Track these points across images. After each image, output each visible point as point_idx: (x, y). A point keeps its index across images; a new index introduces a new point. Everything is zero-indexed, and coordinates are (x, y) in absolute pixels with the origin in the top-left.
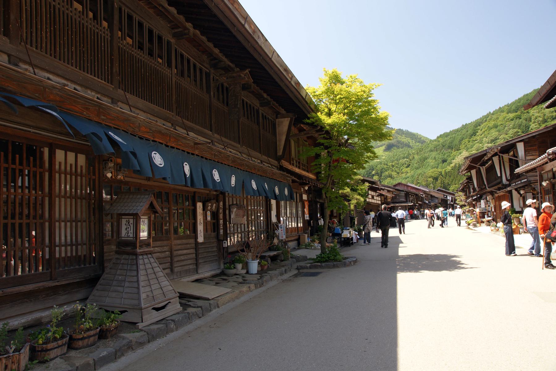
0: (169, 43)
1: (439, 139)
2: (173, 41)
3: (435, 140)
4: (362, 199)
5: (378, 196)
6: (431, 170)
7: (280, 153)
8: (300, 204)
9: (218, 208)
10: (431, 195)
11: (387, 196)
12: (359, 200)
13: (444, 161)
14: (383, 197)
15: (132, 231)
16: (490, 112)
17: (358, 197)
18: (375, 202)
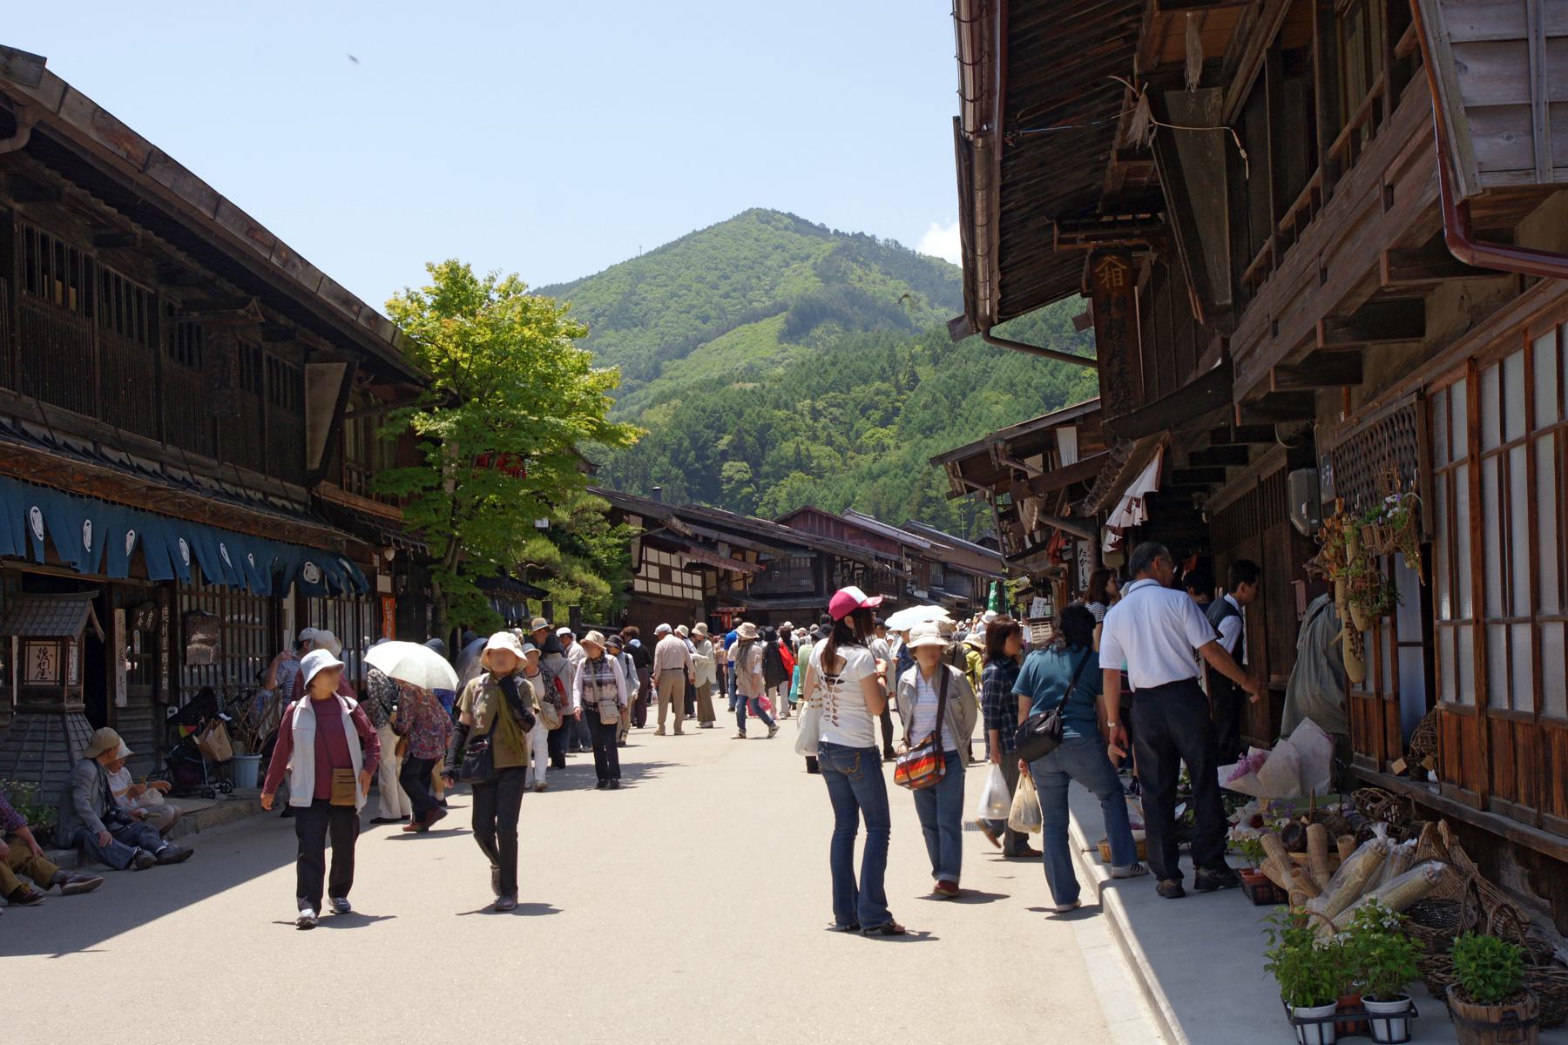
0: (88, 260)
2: (93, 254)
4: (604, 587)
5: (691, 568)
7: (315, 463)
8: (367, 607)
9: (158, 622)
10: (944, 565)
11: (728, 572)
14: (711, 576)
15: (52, 669)
17: (591, 578)
18: (677, 592)
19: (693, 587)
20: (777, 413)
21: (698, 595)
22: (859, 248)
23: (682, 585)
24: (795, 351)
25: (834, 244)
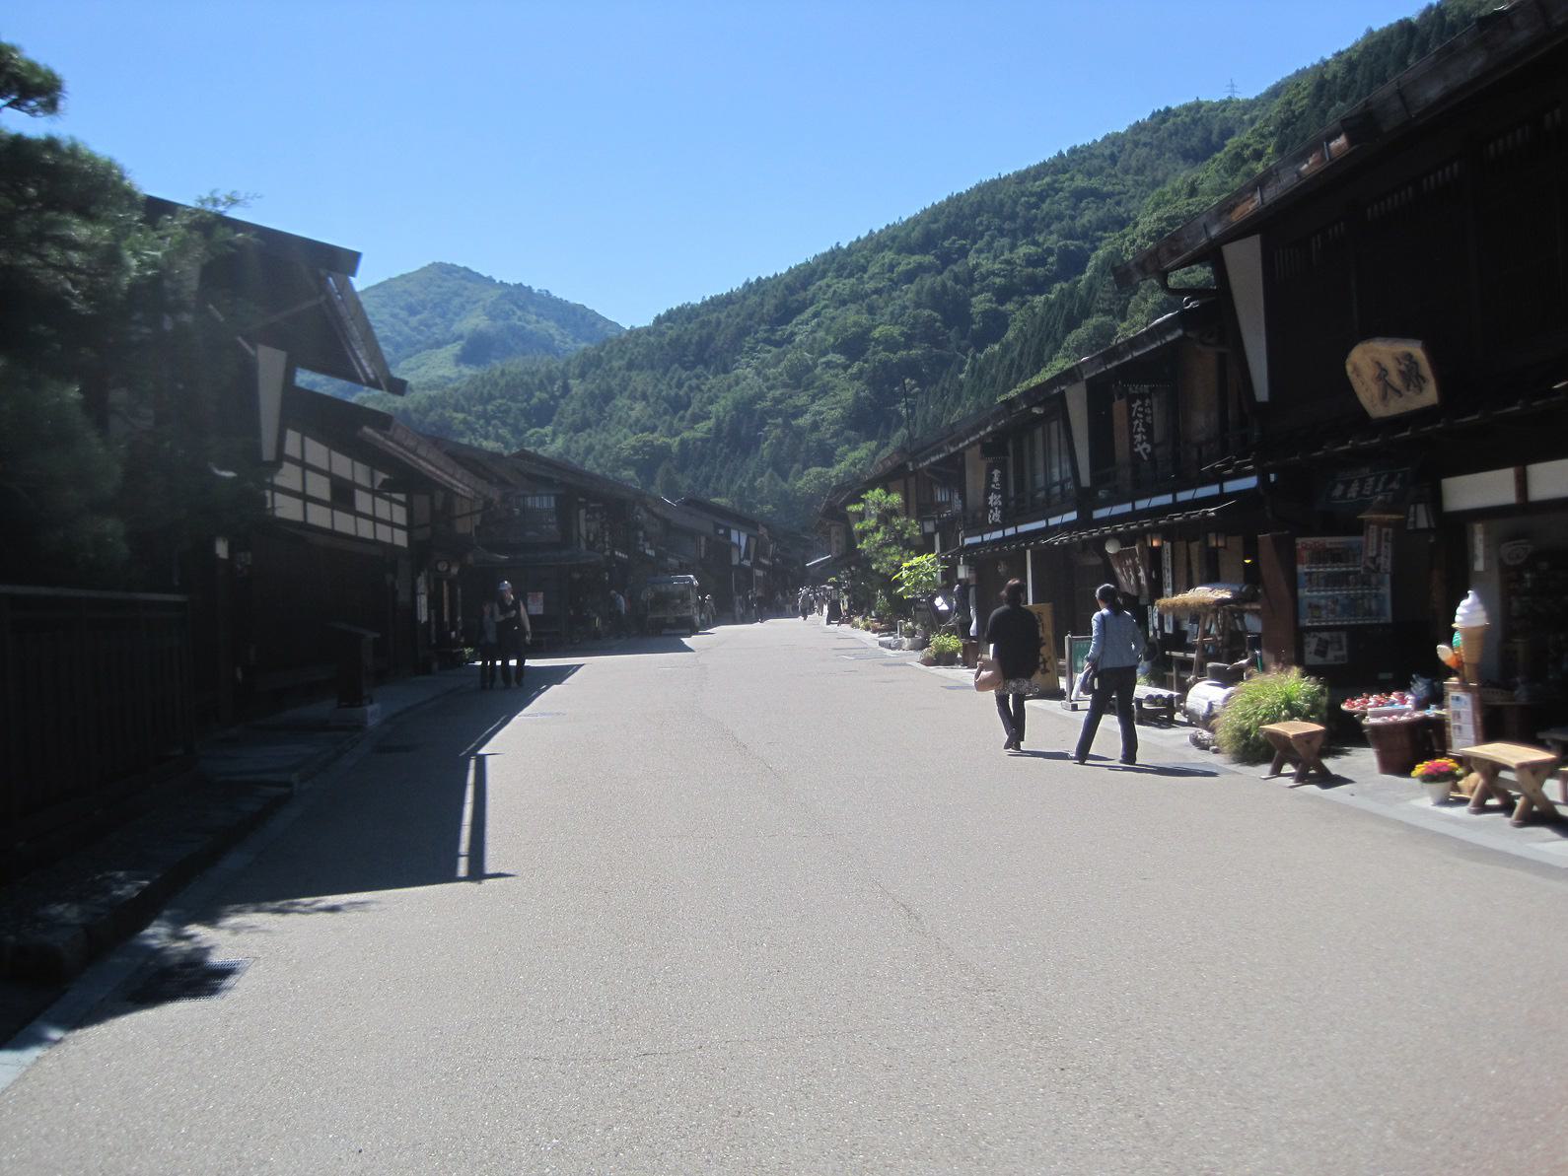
1: (663, 327)
3: (648, 331)
6: (632, 440)
12: (525, 633)
13: (678, 405)
16: (839, 248)
18: (365, 530)
19: (392, 525)
20: (455, 415)
21: (401, 539)
22: (520, 296)
23: (374, 519)
24: (468, 371)
25: (500, 291)
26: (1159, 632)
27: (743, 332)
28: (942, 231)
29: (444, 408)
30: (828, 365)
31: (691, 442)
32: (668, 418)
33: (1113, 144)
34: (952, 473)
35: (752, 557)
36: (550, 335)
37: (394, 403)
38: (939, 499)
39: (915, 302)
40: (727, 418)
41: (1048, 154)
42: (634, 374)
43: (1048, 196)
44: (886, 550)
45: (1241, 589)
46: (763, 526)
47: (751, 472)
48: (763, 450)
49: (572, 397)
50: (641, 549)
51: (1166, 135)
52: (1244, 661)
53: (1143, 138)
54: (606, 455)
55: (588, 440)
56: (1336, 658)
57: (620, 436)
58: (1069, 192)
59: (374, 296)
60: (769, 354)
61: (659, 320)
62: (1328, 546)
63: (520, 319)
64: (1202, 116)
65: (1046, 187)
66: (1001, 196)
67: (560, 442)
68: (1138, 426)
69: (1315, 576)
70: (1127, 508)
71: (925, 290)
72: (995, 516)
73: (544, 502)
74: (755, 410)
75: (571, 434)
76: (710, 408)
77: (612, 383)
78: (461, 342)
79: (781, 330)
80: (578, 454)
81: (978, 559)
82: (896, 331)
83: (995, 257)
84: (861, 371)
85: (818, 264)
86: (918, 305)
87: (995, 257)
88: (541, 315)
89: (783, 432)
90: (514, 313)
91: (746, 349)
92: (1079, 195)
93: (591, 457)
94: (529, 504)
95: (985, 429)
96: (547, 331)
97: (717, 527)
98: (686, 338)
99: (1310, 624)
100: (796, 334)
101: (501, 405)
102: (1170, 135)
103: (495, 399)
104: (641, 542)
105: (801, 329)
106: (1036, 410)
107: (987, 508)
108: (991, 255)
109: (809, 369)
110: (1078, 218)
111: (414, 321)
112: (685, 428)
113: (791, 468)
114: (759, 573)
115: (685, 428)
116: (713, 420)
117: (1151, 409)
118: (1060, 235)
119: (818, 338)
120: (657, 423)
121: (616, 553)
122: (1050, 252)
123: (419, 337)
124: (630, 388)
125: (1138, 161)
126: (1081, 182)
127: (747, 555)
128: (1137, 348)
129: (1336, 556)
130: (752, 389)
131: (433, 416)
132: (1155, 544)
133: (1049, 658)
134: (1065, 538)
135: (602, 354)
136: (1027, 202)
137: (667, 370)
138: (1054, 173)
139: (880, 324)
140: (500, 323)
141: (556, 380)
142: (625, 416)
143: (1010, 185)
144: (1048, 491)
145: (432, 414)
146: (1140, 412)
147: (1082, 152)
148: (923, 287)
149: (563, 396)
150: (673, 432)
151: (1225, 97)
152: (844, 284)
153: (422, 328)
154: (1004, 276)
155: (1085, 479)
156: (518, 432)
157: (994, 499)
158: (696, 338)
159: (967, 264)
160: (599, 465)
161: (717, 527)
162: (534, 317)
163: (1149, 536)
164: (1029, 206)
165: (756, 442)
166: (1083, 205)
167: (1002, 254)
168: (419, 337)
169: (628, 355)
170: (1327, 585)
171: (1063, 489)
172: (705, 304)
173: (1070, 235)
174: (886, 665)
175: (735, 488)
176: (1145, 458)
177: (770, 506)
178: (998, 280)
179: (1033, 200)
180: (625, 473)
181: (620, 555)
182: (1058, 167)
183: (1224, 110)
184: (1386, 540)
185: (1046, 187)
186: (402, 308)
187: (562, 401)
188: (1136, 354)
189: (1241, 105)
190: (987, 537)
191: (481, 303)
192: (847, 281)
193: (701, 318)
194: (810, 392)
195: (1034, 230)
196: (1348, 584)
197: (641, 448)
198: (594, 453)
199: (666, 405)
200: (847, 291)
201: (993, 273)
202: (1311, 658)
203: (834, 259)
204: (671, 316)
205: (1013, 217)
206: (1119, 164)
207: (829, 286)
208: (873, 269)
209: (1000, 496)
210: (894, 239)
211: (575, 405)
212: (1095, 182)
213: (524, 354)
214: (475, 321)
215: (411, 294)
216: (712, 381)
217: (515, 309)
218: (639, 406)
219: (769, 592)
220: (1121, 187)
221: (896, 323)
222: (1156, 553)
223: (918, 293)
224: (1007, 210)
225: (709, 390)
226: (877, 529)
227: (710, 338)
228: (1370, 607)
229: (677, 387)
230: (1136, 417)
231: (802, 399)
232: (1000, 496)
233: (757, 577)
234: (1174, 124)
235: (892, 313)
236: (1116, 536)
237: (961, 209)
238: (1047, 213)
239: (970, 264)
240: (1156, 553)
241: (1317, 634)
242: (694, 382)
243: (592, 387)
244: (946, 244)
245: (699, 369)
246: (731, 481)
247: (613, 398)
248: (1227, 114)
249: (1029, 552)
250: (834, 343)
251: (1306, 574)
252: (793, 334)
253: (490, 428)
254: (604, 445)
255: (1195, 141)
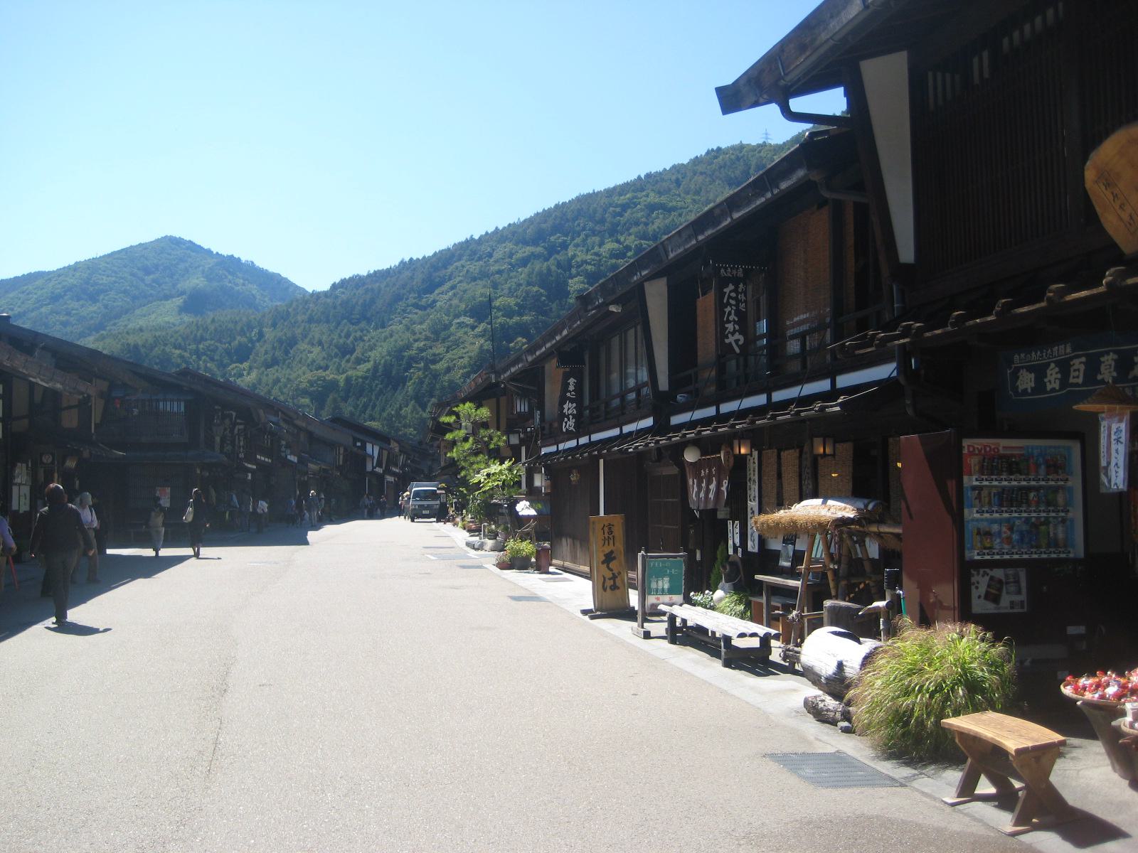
3: (325, 294)
6: (309, 376)
24: (187, 318)
26: (740, 550)
27: (398, 298)
28: (549, 229)
29: (166, 345)
30: (461, 325)
31: (354, 378)
32: (337, 360)
33: (678, 172)
34: (531, 380)
35: (384, 466)
36: (253, 295)
37: (127, 339)
38: (518, 410)
39: (528, 282)
40: (383, 361)
41: (630, 176)
42: (313, 326)
43: (629, 207)
44: (472, 459)
45: (866, 506)
46: (394, 440)
47: (398, 403)
48: (408, 387)
49: (265, 341)
50: (283, 454)
51: (717, 168)
52: (881, 604)
53: (700, 168)
54: (289, 386)
55: (276, 374)
56: (1012, 604)
57: (300, 372)
58: (645, 205)
59: (117, 259)
60: (416, 315)
61: (334, 286)
62: (1002, 452)
63: (230, 282)
64: (744, 155)
65: (628, 201)
66: (595, 205)
67: (254, 375)
68: (730, 314)
69: (985, 493)
70: (710, 411)
71: (535, 273)
72: (570, 424)
73: (175, 407)
74: (404, 357)
75: (263, 369)
76: (370, 353)
77: (296, 332)
78: (184, 297)
79: (426, 298)
80: (267, 385)
81: (555, 470)
82: (512, 301)
83: (588, 251)
84: (485, 330)
85: (456, 250)
86: (529, 284)
87: (588, 251)
88: (247, 280)
89: (423, 373)
90: (226, 277)
91: (399, 310)
92: (652, 208)
93: (277, 387)
94: (168, 409)
95: (561, 334)
96: (250, 292)
97: (355, 440)
98: (354, 301)
99: (979, 558)
100: (437, 301)
101: (210, 345)
102: (720, 167)
103: (206, 340)
104: (283, 449)
105: (442, 297)
106: (613, 308)
107: (562, 416)
108: (584, 249)
109: (446, 327)
110: (651, 224)
111: (148, 279)
112: (350, 368)
113: (429, 401)
114: (390, 479)
115: (350, 368)
116: (372, 362)
117: (745, 296)
118: (636, 237)
119: (453, 305)
120: (329, 364)
121: (270, 461)
122: (628, 248)
123: (152, 292)
124: (310, 336)
125: (696, 185)
126: (653, 198)
127: (379, 464)
128: (738, 208)
129: (1012, 465)
130: (402, 340)
131: (157, 351)
132: (743, 451)
133: (619, 573)
134: (640, 444)
135: (290, 310)
136: (614, 211)
137: (339, 324)
138: (633, 191)
139: (500, 296)
140: (215, 284)
141: (254, 328)
142: (304, 357)
143: (601, 198)
144: (623, 396)
145: (157, 349)
146: (732, 298)
147: (655, 176)
148: (533, 270)
149: (258, 340)
150: (339, 371)
151: (761, 142)
152: (475, 266)
153: (154, 284)
154: (594, 265)
155: (663, 384)
156: (222, 365)
157: (569, 408)
158: (361, 301)
159: (567, 254)
160: (282, 393)
161: (355, 440)
162: (242, 281)
163: (736, 443)
164: (615, 214)
165: (404, 381)
166: (654, 215)
167: (593, 248)
168: (152, 292)
169: (309, 312)
170: (1001, 505)
171: (638, 394)
172: (369, 276)
173: (644, 236)
174: (464, 567)
175: (385, 415)
176: (737, 350)
177: (412, 429)
178: (589, 267)
179: (618, 210)
180: (303, 400)
181: (263, 458)
182: (639, 186)
183: (760, 152)
184: (1118, 441)
185: (628, 201)
186: (139, 269)
187: (257, 344)
188: (736, 215)
189: (772, 148)
190: (561, 447)
191: (201, 268)
192: (476, 264)
193: (366, 287)
194: (447, 344)
195: (617, 232)
196: (1028, 503)
197: (315, 382)
198: (279, 384)
199: (336, 350)
200: (477, 271)
201: (585, 262)
202: (980, 605)
203: (468, 247)
204: (344, 283)
205: (602, 221)
206: (681, 186)
207: (463, 266)
208: (497, 255)
209: (574, 405)
210: (514, 233)
211: (268, 346)
212: (663, 199)
213: (232, 308)
214: (197, 281)
215: (146, 259)
216: (373, 334)
217: (227, 274)
218: (317, 350)
219: (364, 496)
220: (683, 203)
221: (512, 296)
222: (741, 461)
223: (529, 275)
224: (598, 216)
225: (369, 340)
226: (466, 439)
227: (373, 301)
228: (1055, 534)
229: (345, 337)
230: (728, 304)
231: (439, 349)
232: (574, 405)
233: (387, 482)
234: (723, 160)
235: (510, 288)
236: (696, 443)
237: (564, 215)
238: (628, 220)
239: (570, 254)
240: (741, 461)
241: (988, 571)
242: (359, 334)
243: (280, 334)
244: (552, 239)
245: (363, 324)
246: (383, 410)
247: (296, 343)
248: (762, 154)
249: (601, 461)
250: (465, 308)
251: (974, 488)
252: (435, 301)
253: (201, 362)
254: (288, 379)
255: (738, 173)
